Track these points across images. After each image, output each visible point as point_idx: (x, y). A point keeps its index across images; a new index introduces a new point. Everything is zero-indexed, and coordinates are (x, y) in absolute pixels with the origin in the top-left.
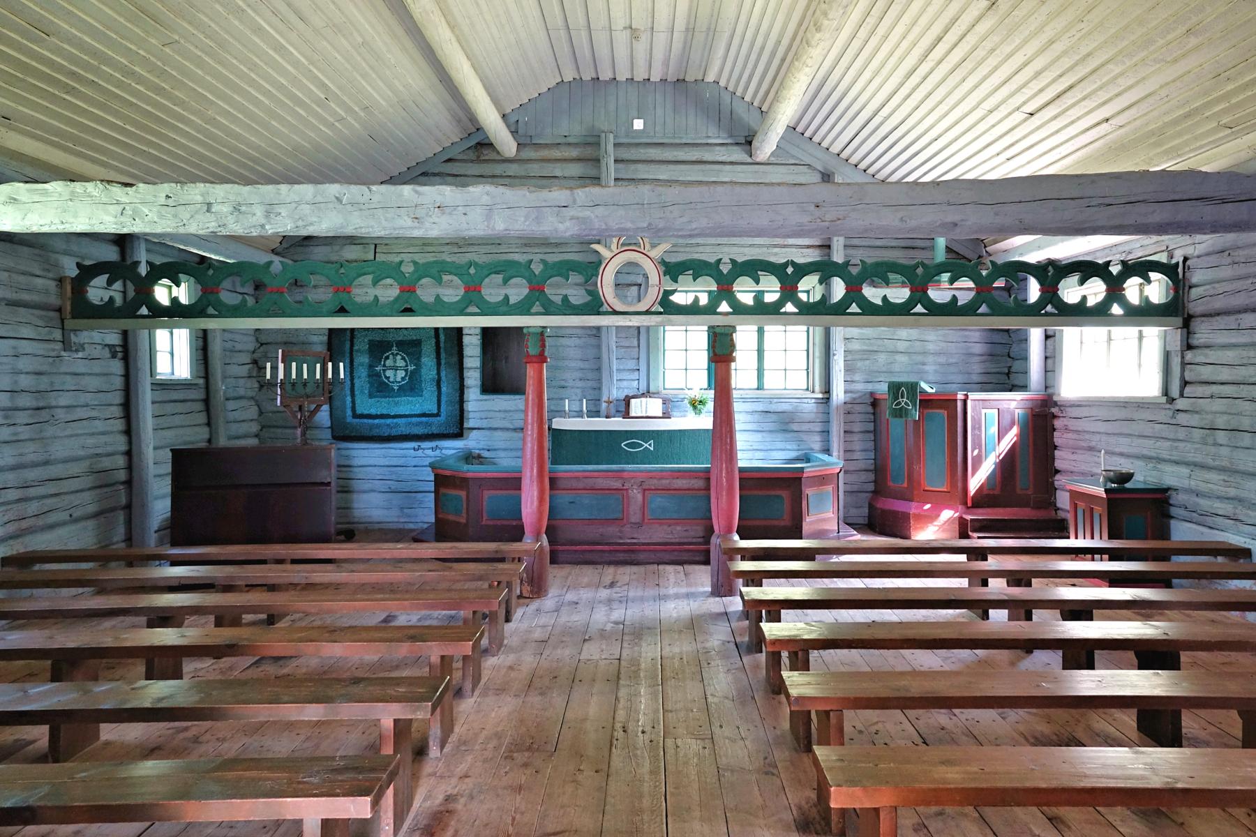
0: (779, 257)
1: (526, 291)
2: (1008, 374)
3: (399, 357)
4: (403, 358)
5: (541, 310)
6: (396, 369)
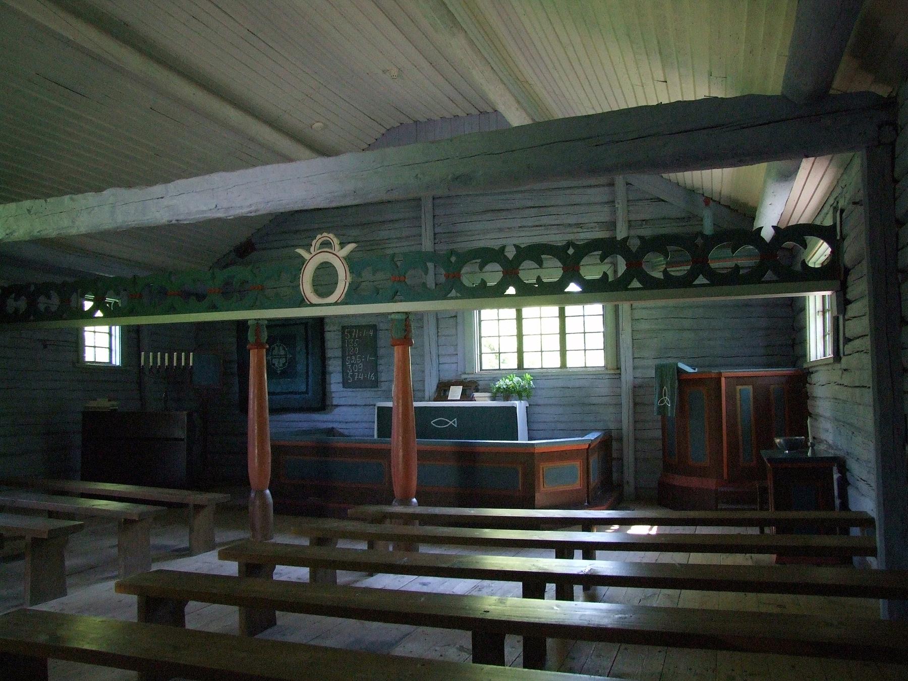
0: (557, 238)
1: (501, 275)
2: (793, 346)
3: (281, 348)
4: (284, 349)
5: (775, 278)
6: (280, 357)
